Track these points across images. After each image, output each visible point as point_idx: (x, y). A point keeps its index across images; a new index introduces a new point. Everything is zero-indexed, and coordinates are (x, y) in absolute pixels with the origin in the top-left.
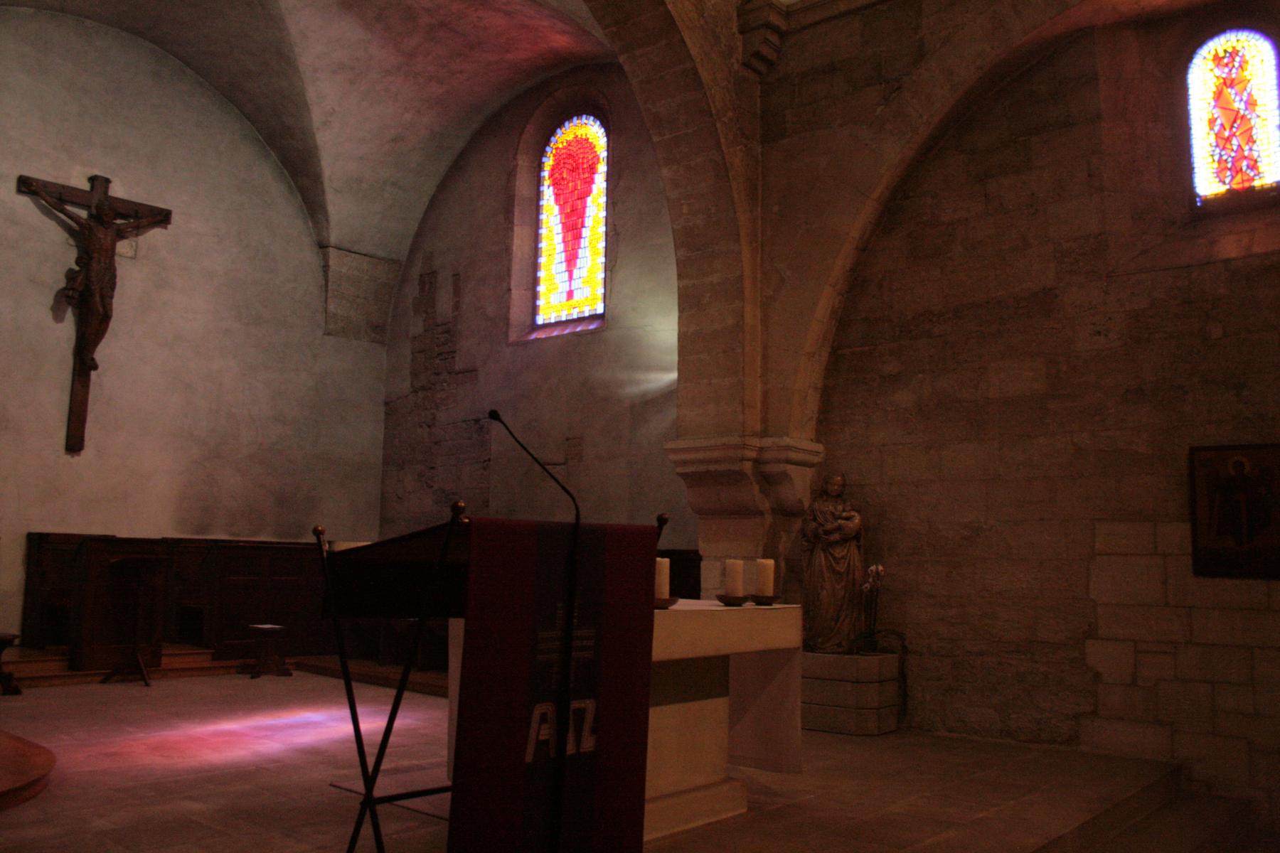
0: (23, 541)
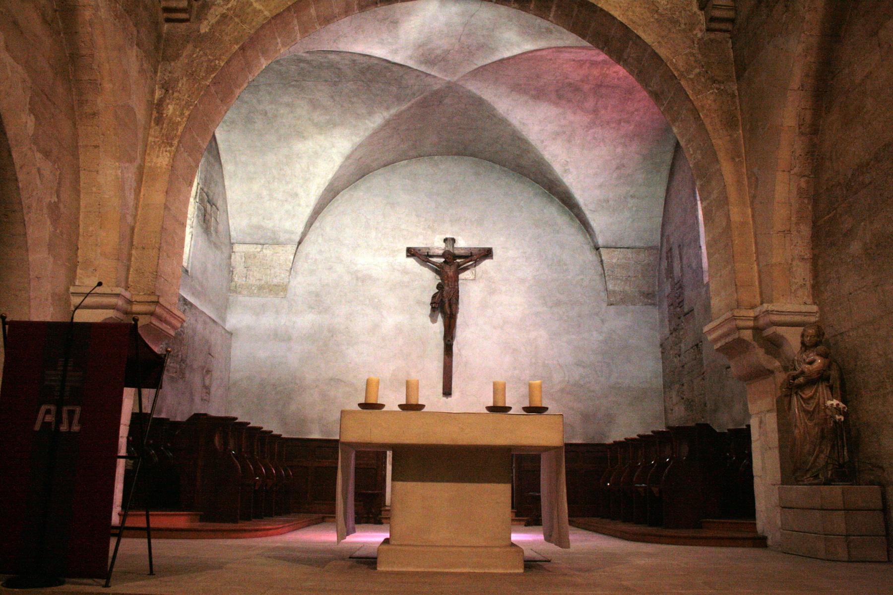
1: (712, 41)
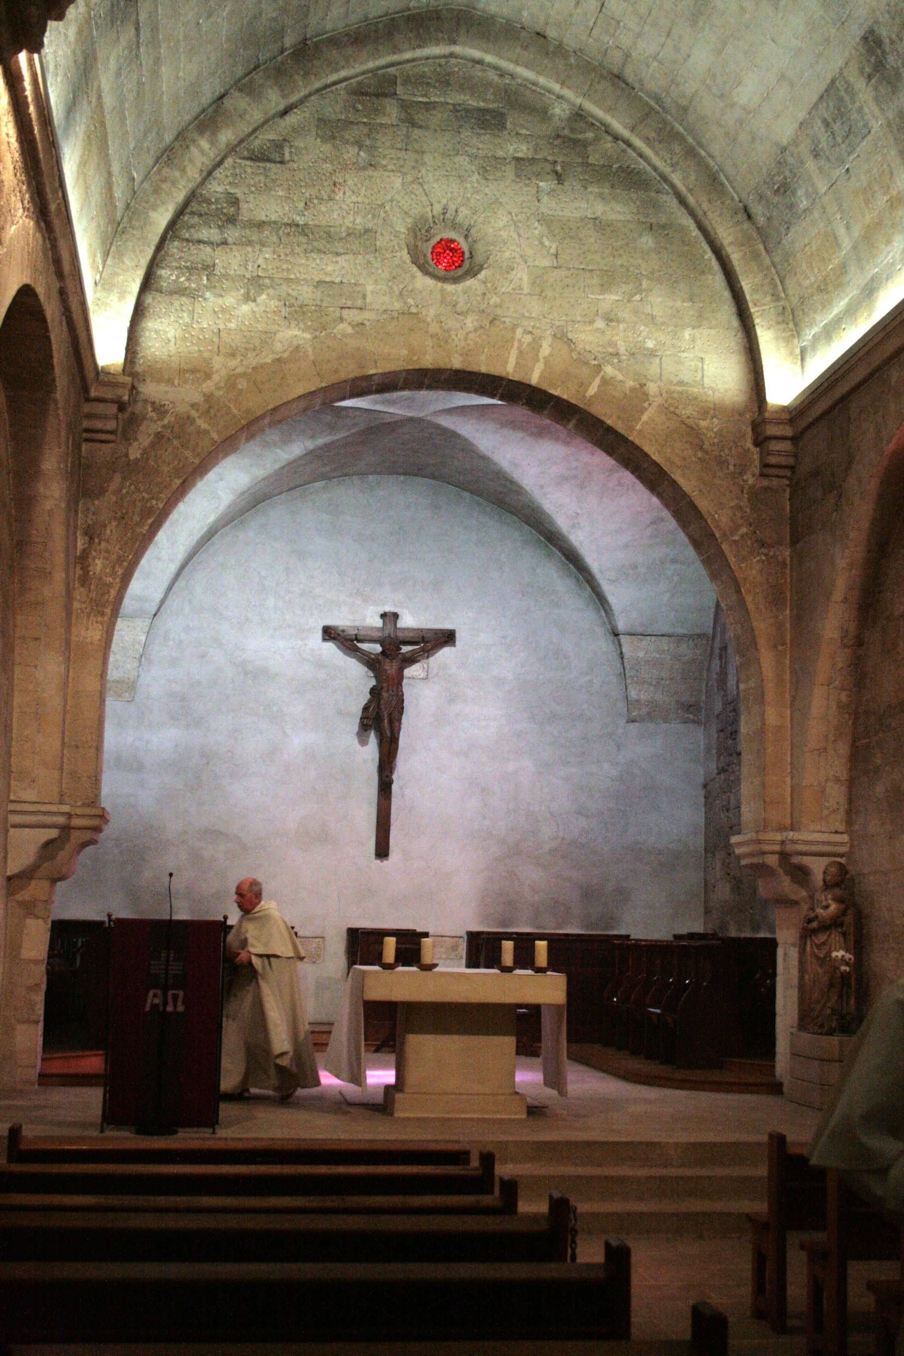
0: (345, 934)
1: (766, 489)
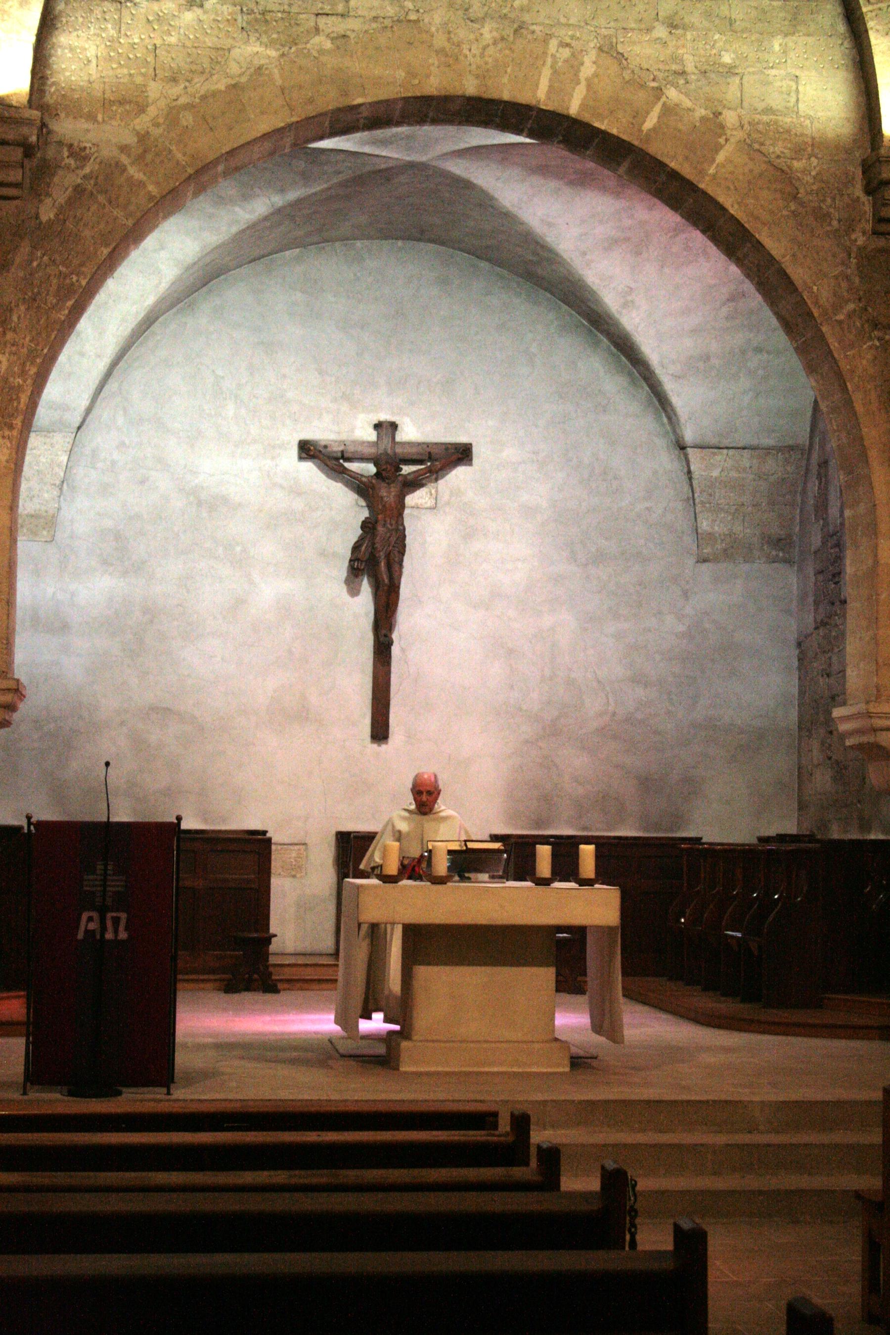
0: (332, 840)
